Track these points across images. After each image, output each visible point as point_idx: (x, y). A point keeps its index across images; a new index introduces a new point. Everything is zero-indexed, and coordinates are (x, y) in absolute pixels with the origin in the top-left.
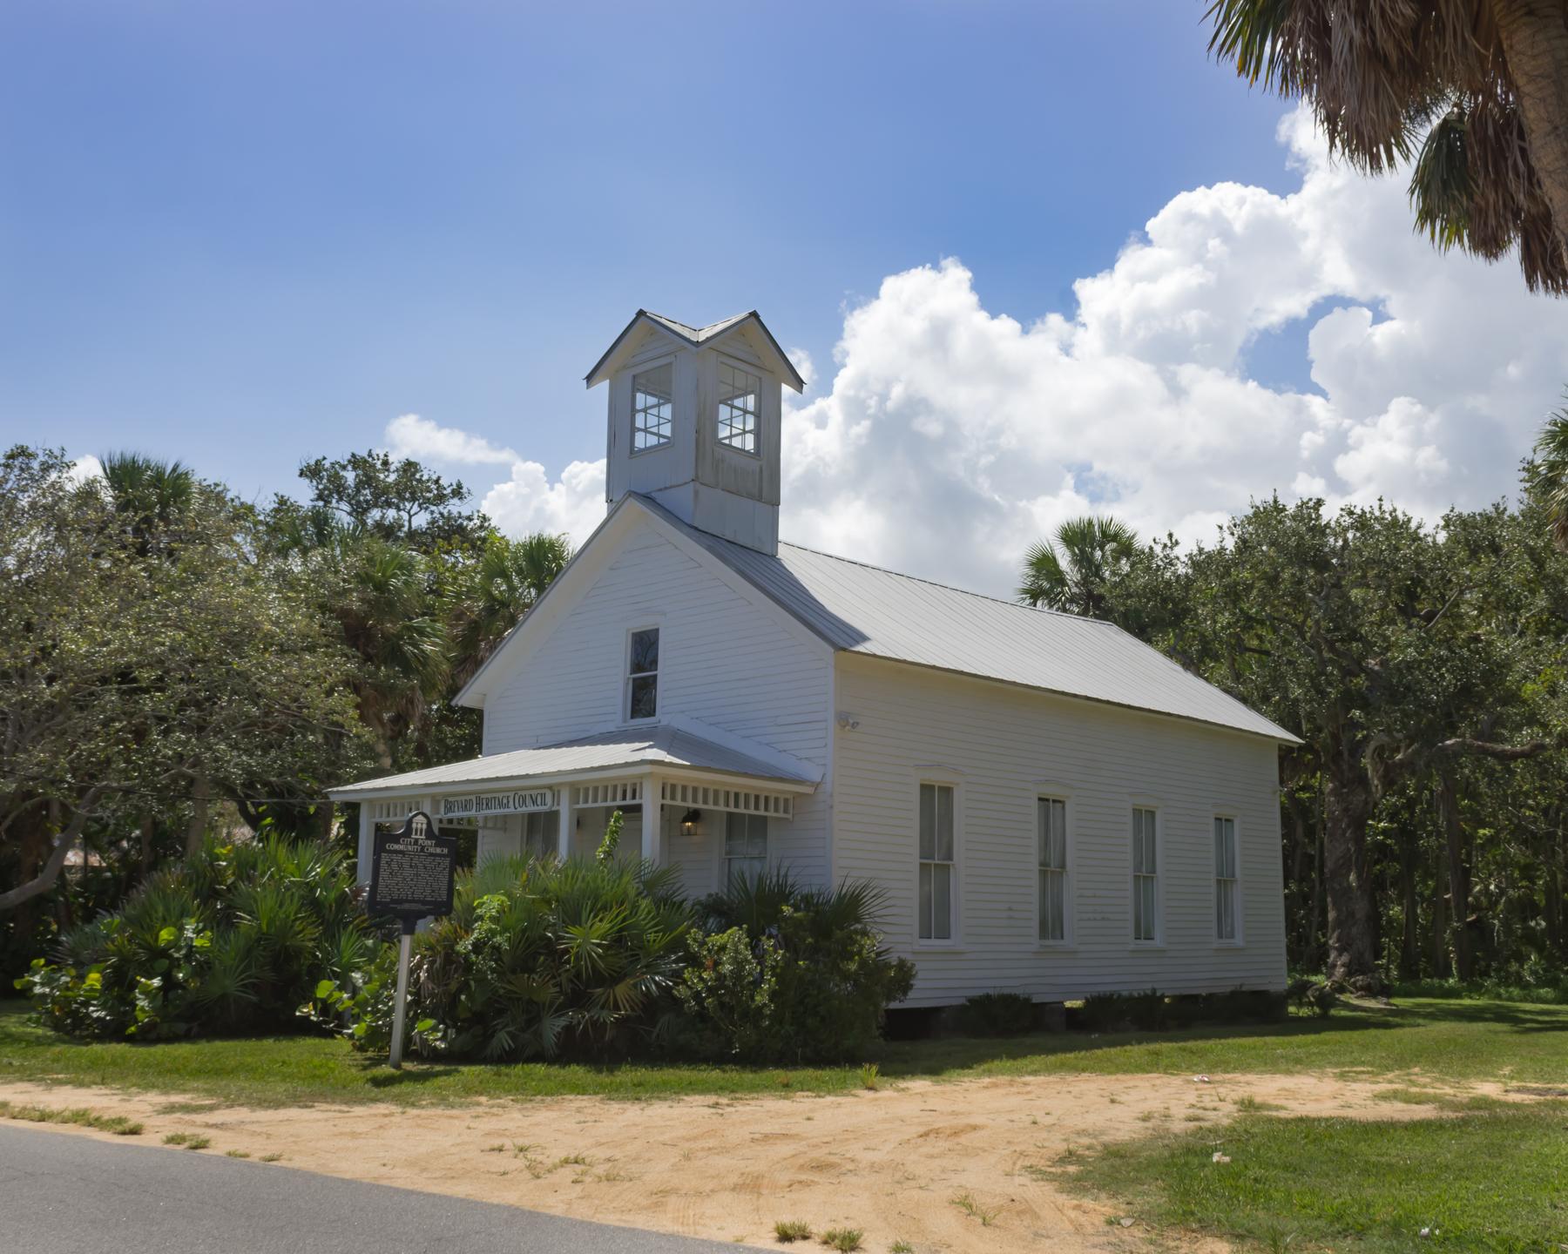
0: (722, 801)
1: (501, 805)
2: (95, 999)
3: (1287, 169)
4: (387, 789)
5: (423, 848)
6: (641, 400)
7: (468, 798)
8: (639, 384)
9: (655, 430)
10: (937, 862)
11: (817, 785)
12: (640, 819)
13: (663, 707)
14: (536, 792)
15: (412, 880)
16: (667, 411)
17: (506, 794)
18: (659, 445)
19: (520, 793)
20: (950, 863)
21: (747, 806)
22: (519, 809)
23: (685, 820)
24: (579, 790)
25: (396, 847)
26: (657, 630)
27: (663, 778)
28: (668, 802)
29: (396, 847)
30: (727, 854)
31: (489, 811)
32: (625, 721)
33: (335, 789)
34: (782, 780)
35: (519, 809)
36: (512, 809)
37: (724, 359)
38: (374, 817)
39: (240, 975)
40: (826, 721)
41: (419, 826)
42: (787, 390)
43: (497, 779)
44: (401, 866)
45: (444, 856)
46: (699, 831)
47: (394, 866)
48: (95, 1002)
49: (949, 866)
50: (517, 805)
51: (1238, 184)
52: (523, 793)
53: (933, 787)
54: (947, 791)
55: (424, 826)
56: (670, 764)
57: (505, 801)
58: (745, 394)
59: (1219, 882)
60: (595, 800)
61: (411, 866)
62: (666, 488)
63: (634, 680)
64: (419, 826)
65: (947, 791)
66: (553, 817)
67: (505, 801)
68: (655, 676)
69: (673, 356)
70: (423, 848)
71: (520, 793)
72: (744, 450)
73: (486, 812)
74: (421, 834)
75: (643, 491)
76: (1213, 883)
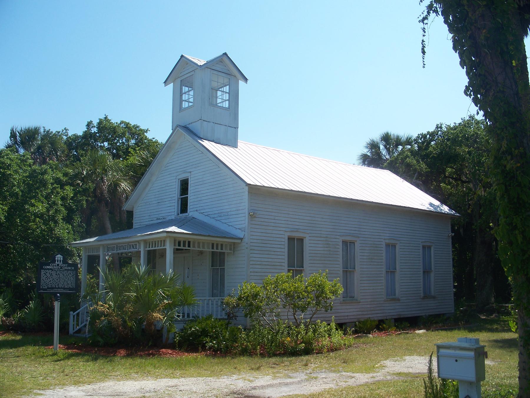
0: (196, 246)
5: (61, 268)
6: (185, 89)
7: (113, 246)
8: (183, 83)
9: (224, 93)
10: (391, 270)
11: (241, 239)
13: (175, 209)
15: (57, 280)
16: (192, 93)
18: (189, 106)
19: (129, 244)
20: (396, 270)
21: (217, 249)
24: (159, 241)
25: (48, 267)
27: (174, 238)
29: (48, 267)
31: (120, 251)
34: (225, 237)
40: (245, 213)
41: (59, 259)
42: (241, 83)
44: (51, 275)
45: (73, 270)
47: (48, 274)
49: (224, 268)
53: (294, 239)
54: (301, 240)
55: (62, 259)
56: (183, 233)
58: (226, 86)
59: (424, 272)
61: (56, 275)
63: (181, 198)
64: (59, 259)
65: (301, 240)
66: (163, 254)
68: (187, 197)
69: (194, 71)
70: (61, 268)
71: (129, 244)
72: (225, 107)
74: (60, 262)
75: (183, 125)
76: (422, 273)
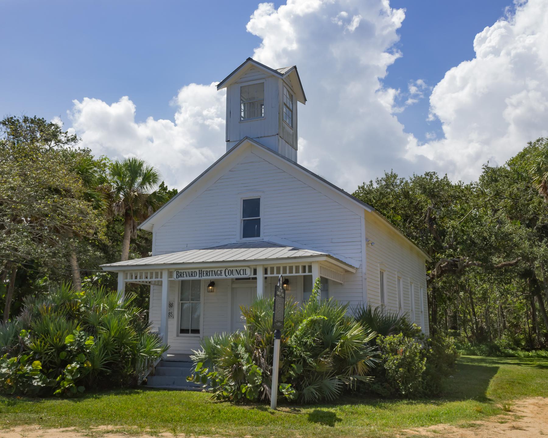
1: (216, 274)
2: (36, 375)
3: (125, 98)
4: (128, 266)
12: (256, 282)
14: (190, 271)
17: (220, 269)
19: (229, 269)
22: (228, 276)
23: (209, 286)
26: (259, 199)
28: (269, 275)
30: (181, 300)
32: (241, 239)
33: (105, 265)
35: (228, 276)
36: (224, 276)
37: (284, 84)
38: (126, 278)
39: (104, 357)
43: (183, 263)
46: (290, 288)
48: (37, 377)
50: (227, 274)
51: (104, 103)
52: (231, 269)
57: (219, 272)
60: (151, 278)
62: (261, 137)
63: (244, 220)
67: (219, 272)
71: (229, 269)
73: (205, 277)
